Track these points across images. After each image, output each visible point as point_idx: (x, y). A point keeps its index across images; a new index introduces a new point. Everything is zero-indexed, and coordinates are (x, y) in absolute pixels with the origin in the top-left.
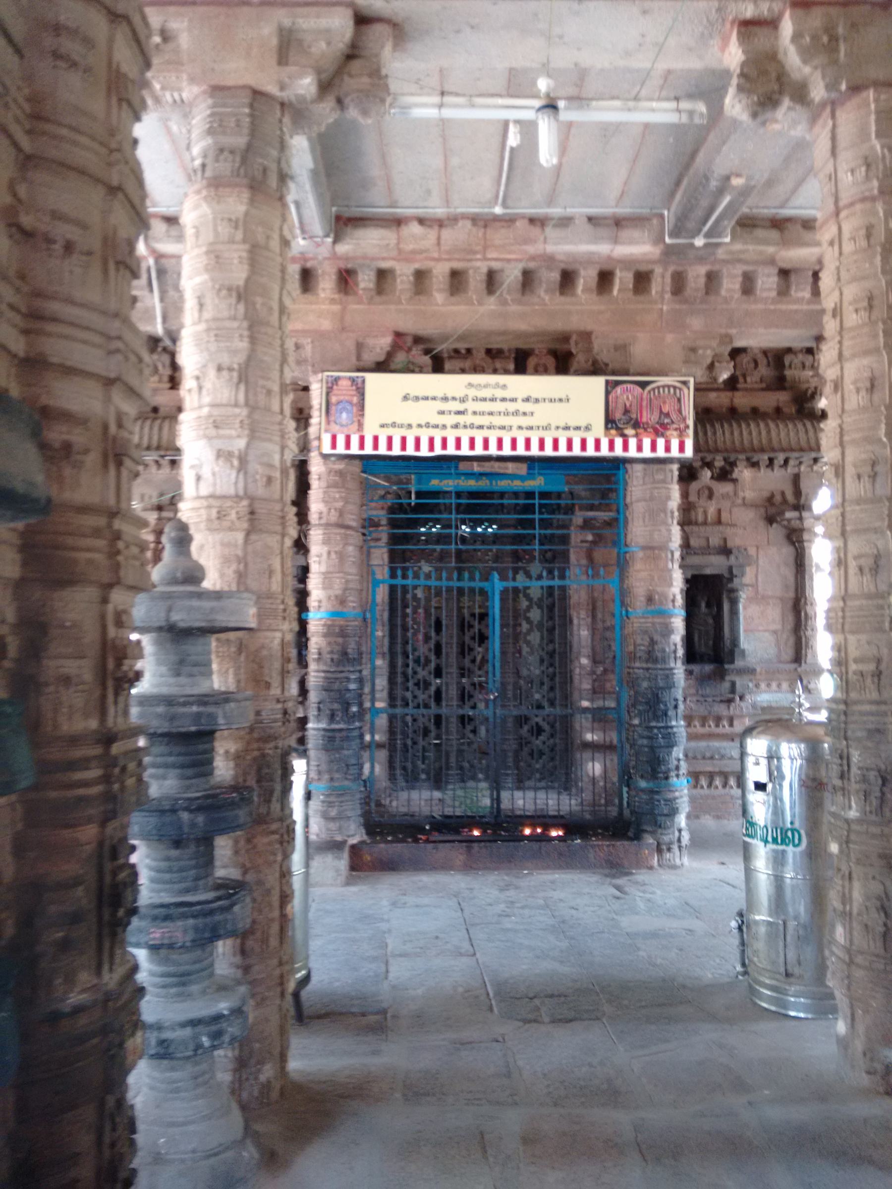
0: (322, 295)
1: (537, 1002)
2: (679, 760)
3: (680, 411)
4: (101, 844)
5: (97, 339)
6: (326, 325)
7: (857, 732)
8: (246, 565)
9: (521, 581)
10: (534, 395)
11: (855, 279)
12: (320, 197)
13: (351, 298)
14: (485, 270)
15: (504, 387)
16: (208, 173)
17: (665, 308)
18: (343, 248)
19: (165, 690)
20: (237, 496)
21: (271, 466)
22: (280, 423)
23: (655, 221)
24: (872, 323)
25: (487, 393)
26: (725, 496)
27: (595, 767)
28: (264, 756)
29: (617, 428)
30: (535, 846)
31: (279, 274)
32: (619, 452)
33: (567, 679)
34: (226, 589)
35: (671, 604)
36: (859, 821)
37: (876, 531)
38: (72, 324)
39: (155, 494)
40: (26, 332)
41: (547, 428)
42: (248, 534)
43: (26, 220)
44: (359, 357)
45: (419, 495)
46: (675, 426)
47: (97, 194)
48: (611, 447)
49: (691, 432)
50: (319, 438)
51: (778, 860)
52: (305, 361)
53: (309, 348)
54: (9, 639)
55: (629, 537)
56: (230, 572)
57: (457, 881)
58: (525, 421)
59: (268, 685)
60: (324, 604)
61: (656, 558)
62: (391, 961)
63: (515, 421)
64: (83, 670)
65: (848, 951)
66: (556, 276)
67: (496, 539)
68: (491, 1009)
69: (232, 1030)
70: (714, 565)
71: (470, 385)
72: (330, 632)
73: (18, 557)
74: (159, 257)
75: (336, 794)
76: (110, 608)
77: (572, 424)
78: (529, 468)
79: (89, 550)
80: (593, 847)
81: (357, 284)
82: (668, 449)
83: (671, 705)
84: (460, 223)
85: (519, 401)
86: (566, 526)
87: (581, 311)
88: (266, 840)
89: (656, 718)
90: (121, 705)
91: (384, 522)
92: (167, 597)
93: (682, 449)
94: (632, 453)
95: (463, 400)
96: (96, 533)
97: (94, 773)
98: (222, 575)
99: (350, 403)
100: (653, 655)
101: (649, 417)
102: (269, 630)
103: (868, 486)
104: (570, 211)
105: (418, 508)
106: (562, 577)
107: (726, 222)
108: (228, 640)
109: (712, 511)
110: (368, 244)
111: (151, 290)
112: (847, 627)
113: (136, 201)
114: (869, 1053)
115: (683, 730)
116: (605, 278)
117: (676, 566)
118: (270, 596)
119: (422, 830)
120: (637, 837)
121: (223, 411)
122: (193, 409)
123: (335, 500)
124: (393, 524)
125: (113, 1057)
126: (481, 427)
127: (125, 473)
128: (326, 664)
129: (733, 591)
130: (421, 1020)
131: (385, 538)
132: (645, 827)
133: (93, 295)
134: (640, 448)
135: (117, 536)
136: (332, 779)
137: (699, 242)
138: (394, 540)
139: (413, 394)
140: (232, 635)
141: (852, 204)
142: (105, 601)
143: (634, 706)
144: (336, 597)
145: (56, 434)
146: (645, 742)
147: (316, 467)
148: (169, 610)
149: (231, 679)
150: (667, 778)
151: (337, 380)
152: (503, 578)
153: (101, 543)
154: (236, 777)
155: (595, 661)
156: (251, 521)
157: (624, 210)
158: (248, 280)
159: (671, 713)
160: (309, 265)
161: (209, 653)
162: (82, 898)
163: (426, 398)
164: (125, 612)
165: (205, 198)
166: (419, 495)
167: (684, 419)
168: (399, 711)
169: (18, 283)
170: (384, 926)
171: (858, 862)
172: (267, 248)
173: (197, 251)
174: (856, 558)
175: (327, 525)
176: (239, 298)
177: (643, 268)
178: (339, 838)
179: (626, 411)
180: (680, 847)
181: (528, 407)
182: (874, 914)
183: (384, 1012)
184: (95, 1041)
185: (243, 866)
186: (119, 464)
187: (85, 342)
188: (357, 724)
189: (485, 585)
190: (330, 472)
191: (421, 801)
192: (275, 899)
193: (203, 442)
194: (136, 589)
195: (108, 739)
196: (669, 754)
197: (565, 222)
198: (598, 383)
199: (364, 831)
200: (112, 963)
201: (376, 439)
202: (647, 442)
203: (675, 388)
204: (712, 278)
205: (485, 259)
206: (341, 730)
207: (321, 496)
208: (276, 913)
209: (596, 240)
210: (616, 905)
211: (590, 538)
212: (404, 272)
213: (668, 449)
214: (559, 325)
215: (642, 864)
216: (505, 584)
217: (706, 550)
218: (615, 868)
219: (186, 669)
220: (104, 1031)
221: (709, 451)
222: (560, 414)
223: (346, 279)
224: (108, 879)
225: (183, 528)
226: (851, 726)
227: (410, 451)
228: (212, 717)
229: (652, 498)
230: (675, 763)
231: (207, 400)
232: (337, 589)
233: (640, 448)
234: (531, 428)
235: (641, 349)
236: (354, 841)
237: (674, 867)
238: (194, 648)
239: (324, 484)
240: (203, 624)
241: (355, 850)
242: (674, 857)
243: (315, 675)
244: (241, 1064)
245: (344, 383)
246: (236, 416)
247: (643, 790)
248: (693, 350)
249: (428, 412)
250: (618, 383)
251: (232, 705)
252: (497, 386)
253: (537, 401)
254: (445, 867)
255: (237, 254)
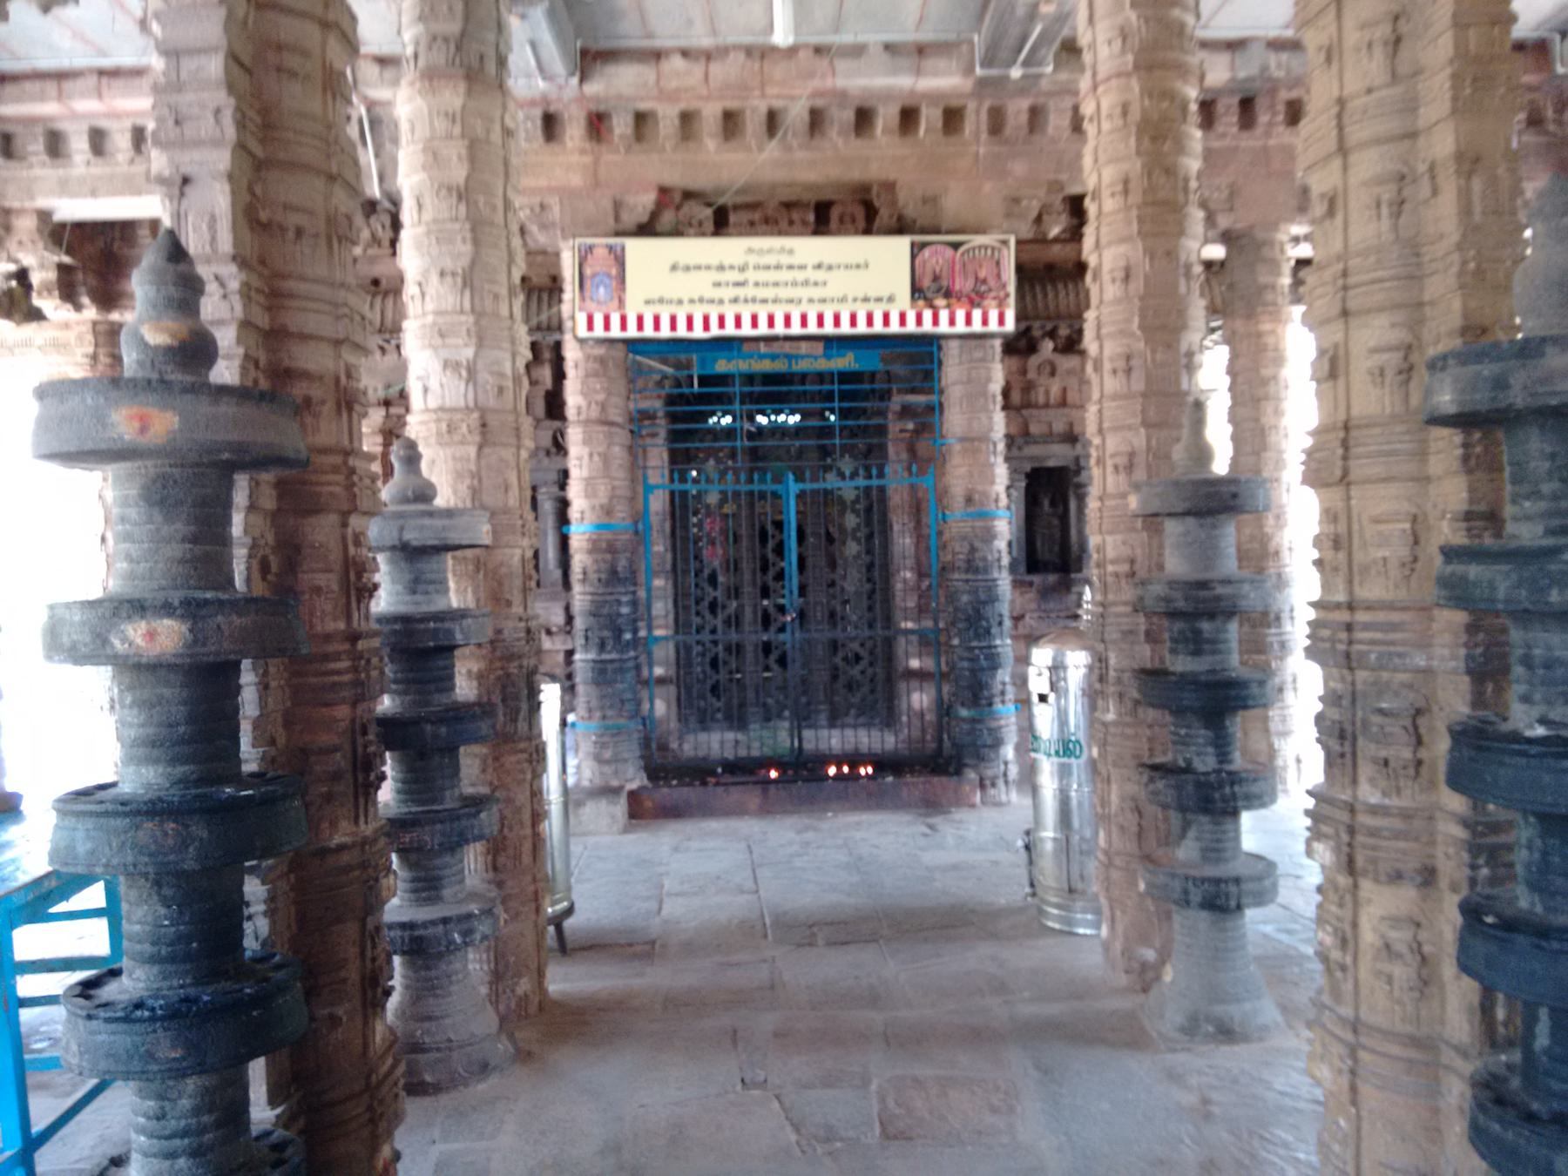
0: (569, 144)
1: (815, 929)
2: (1004, 684)
3: (999, 276)
4: (353, 721)
5: (327, 308)
6: (576, 180)
7: (1112, 634)
8: (480, 480)
9: (831, 481)
10: (826, 261)
11: (1110, 161)
12: (559, 35)
13: (604, 148)
14: (763, 109)
15: (791, 252)
16: (421, 63)
17: (982, 150)
18: (594, 88)
19: (402, 609)
20: (467, 408)
21: (502, 375)
22: (510, 329)
23: (965, 48)
24: (1127, 208)
25: (771, 260)
26: (1070, 372)
27: (920, 699)
28: (508, 675)
29: (925, 299)
30: (841, 785)
31: (501, 168)
32: (927, 327)
33: (888, 599)
34: (460, 505)
35: (993, 506)
36: (1115, 723)
37: (1129, 428)
38: (307, 298)
39: (380, 387)
40: (269, 309)
41: (843, 300)
42: (480, 448)
43: (264, 216)
44: (617, 218)
45: (704, 381)
46: (993, 294)
47: (319, 183)
48: (919, 321)
49: (1012, 300)
50: (573, 318)
51: (1064, 772)
52: (553, 224)
53: (556, 209)
54: (272, 558)
55: (946, 426)
56: (463, 488)
57: (750, 826)
58: (817, 293)
59: (509, 604)
60: (587, 515)
61: (976, 451)
62: (666, 899)
63: (804, 293)
64: (330, 581)
65: (1106, 853)
66: (849, 115)
67: (797, 431)
68: (765, 936)
69: (483, 928)
70: (1057, 454)
71: (750, 251)
72: (594, 548)
73: (274, 493)
74: (371, 105)
75: (608, 736)
76: (350, 530)
77: (872, 294)
78: (825, 348)
79: (329, 484)
80: (907, 784)
81: (611, 130)
82: (985, 322)
83: (994, 622)
84: (732, 55)
85: (809, 268)
86: (882, 413)
87: (881, 158)
88: (513, 758)
89: (978, 636)
90: (363, 611)
91: (660, 414)
92: (400, 515)
93: (1001, 321)
94: (944, 327)
95: (743, 269)
96: (335, 469)
97: (344, 664)
98: (455, 492)
99: (609, 275)
100: (975, 565)
101: (963, 284)
102: (507, 546)
103: (1124, 381)
104: (861, 38)
105: (701, 398)
106: (881, 475)
107: (1043, 51)
108: (465, 558)
109: (1055, 390)
110: (621, 84)
111: (365, 143)
112: (1104, 527)
113: (353, 182)
114: (1127, 952)
115: (1009, 649)
116: (909, 117)
117: (1000, 459)
118: (506, 511)
119: (713, 773)
120: (958, 772)
121: (448, 319)
122: (416, 317)
123: (596, 392)
124: (673, 418)
125: (371, 888)
126: (764, 301)
127: (355, 416)
128: (592, 585)
129: (1080, 486)
130: (692, 948)
131: (663, 433)
132: (967, 761)
133: (321, 270)
134: (952, 322)
135: (352, 471)
136: (604, 717)
137: (1016, 73)
138: (674, 436)
139: (682, 263)
140: (469, 553)
141: (1108, 79)
142: (345, 525)
143: (953, 624)
144: (602, 507)
145: (299, 390)
146: (965, 664)
147: (571, 353)
148: (402, 529)
149: (470, 595)
150: (990, 705)
151: (591, 248)
152: (800, 478)
153: (339, 478)
154: (480, 696)
155: (921, 574)
156: (483, 434)
157: (927, 36)
158: (468, 179)
159: (994, 630)
160: (552, 109)
161: (445, 571)
162: (340, 760)
163: (698, 268)
164: (363, 533)
165: (420, 92)
166: (704, 381)
167: (1004, 286)
168: (692, 639)
169: (260, 268)
170: (662, 869)
171: (1115, 765)
172: (488, 141)
173: (412, 148)
174: (1112, 456)
175: (587, 422)
176: (460, 198)
177: (954, 103)
178: (615, 783)
179: (936, 278)
180: (1006, 782)
181: (820, 275)
182: (1129, 815)
183: (653, 943)
184: (357, 873)
185: (491, 784)
186: (350, 409)
187: (317, 311)
188: (632, 654)
189: (779, 488)
190: (588, 358)
191: (717, 743)
192: (526, 816)
193: (428, 353)
194: (370, 514)
195: (354, 637)
196: (993, 676)
197: (857, 51)
198: (902, 244)
199: (644, 775)
200: (366, 817)
201: (640, 319)
202: (960, 315)
203: (993, 249)
204: (1036, 115)
205: (763, 95)
206: (612, 661)
207: (579, 387)
208: (528, 831)
209: (895, 72)
210: (922, 842)
211: (910, 426)
212: (668, 116)
213: (985, 322)
214: (856, 175)
215: (961, 802)
216: (801, 486)
217: (1049, 438)
218: (932, 806)
219: (421, 587)
220: (364, 866)
221: (1049, 318)
222: (852, 284)
223: (597, 123)
224: (360, 750)
225: (411, 445)
226: (1108, 629)
227: (682, 332)
228: (450, 633)
229: (969, 381)
230: (1000, 687)
231: (430, 306)
232: (603, 498)
233: (952, 322)
234: (823, 301)
235: (954, 202)
236: (633, 786)
237: (999, 804)
238: (429, 566)
239: (581, 372)
240: (436, 542)
241: (633, 797)
242: (1000, 792)
243: (580, 597)
244: (497, 977)
245: (600, 252)
246: (461, 324)
247: (963, 720)
248: (1016, 200)
249: (700, 284)
250: (924, 245)
251: (470, 620)
252: (782, 250)
253: (830, 268)
254: (738, 811)
255: (455, 151)
